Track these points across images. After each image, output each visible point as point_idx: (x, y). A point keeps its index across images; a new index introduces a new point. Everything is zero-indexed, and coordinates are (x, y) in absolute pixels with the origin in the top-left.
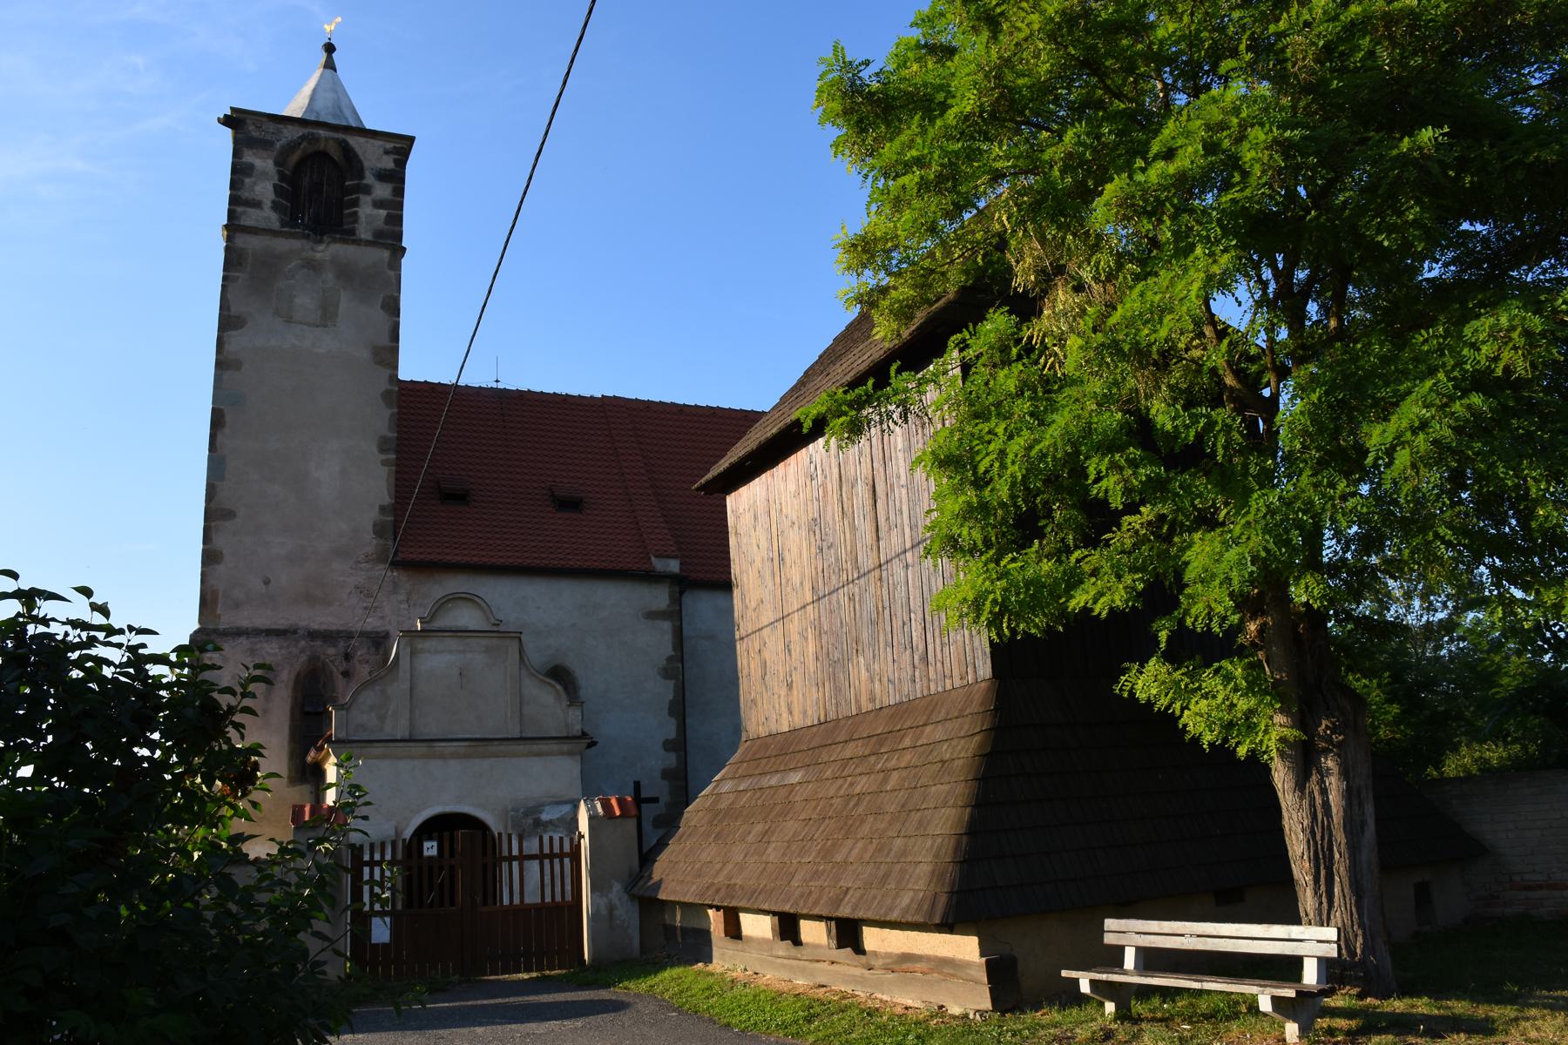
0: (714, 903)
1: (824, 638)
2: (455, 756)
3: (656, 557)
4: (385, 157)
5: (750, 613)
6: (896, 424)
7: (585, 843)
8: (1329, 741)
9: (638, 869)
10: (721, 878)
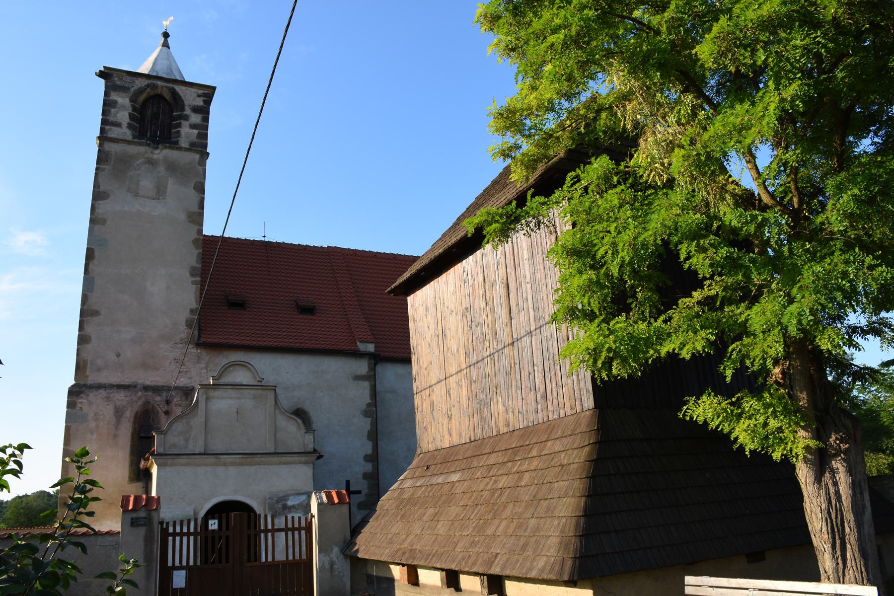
0: (401, 562)
1: (474, 385)
2: (233, 464)
3: (360, 342)
5: (423, 370)
6: (532, 230)
7: (315, 521)
9: (350, 538)
10: (406, 545)
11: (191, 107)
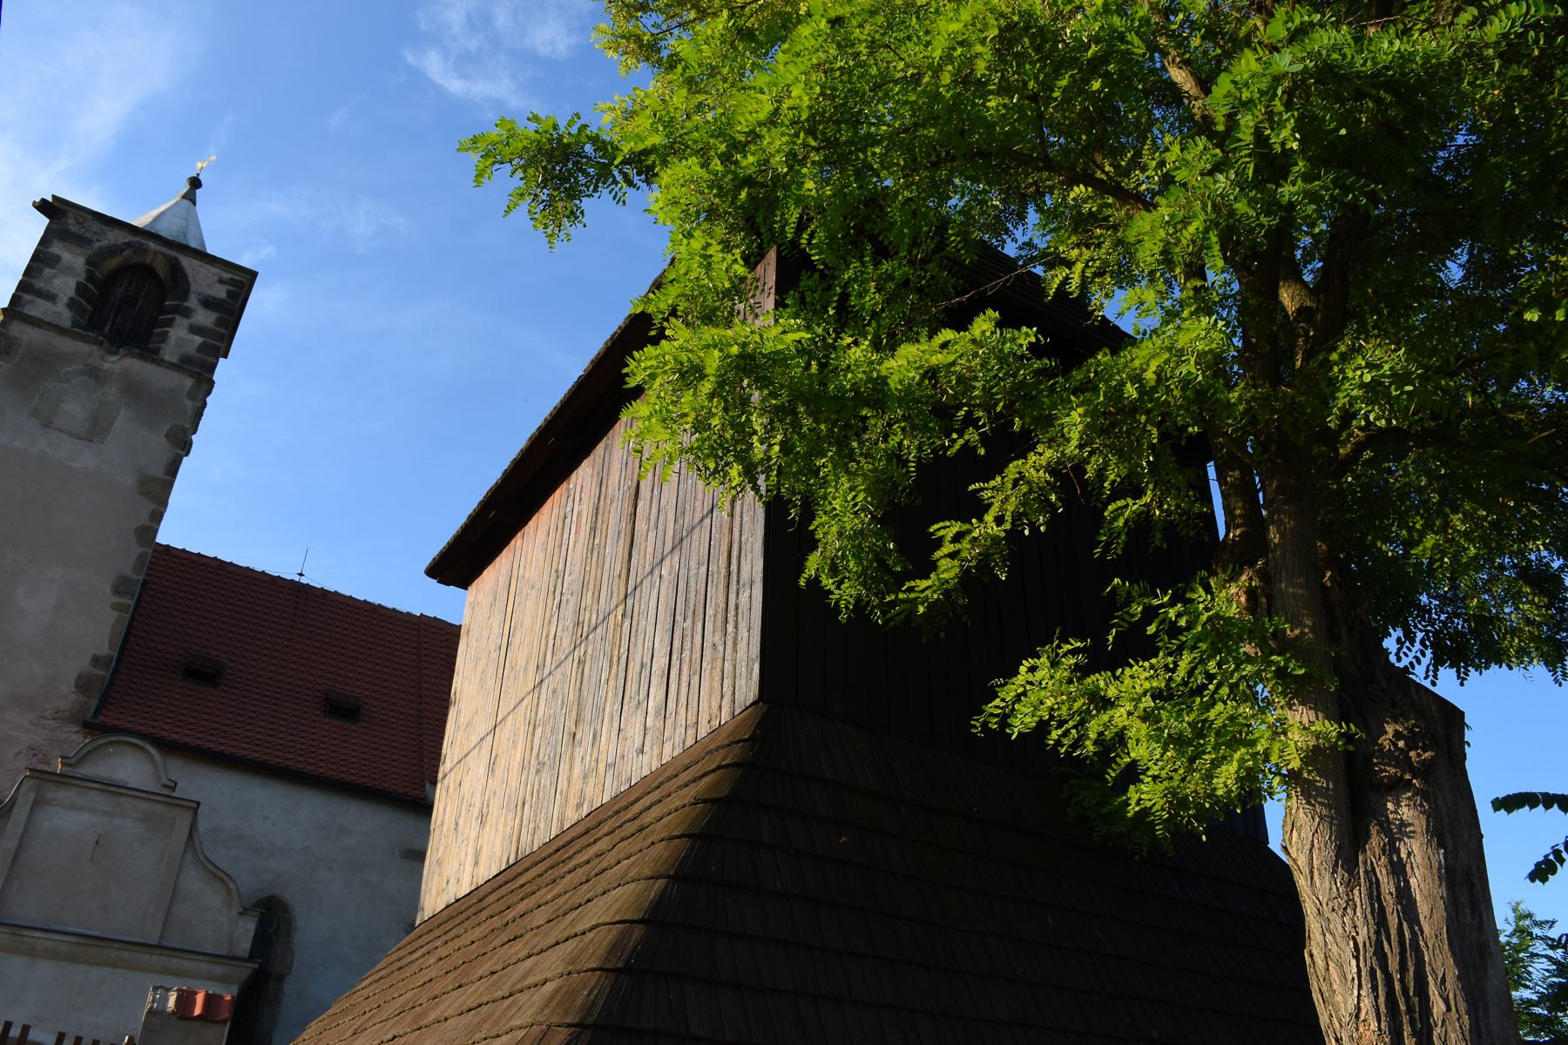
2: (53, 955)
4: (219, 286)
8: (1405, 763)
11: (200, 297)
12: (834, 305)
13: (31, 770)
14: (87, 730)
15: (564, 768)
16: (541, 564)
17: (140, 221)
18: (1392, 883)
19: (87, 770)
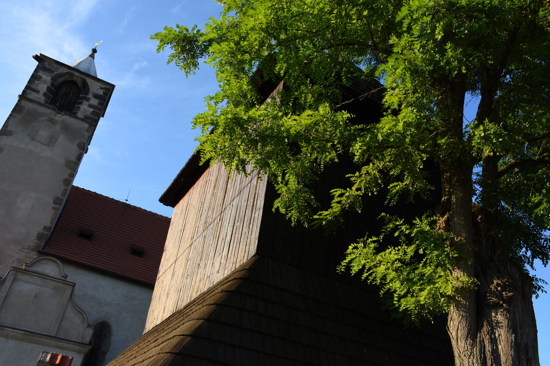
2: (15, 338)
8: (500, 297)
12: (292, 102)
13: (13, 267)
14: (40, 254)
15: (195, 277)
16: (198, 199)
17: (72, 64)
18: (490, 347)
19: (34, 269)
